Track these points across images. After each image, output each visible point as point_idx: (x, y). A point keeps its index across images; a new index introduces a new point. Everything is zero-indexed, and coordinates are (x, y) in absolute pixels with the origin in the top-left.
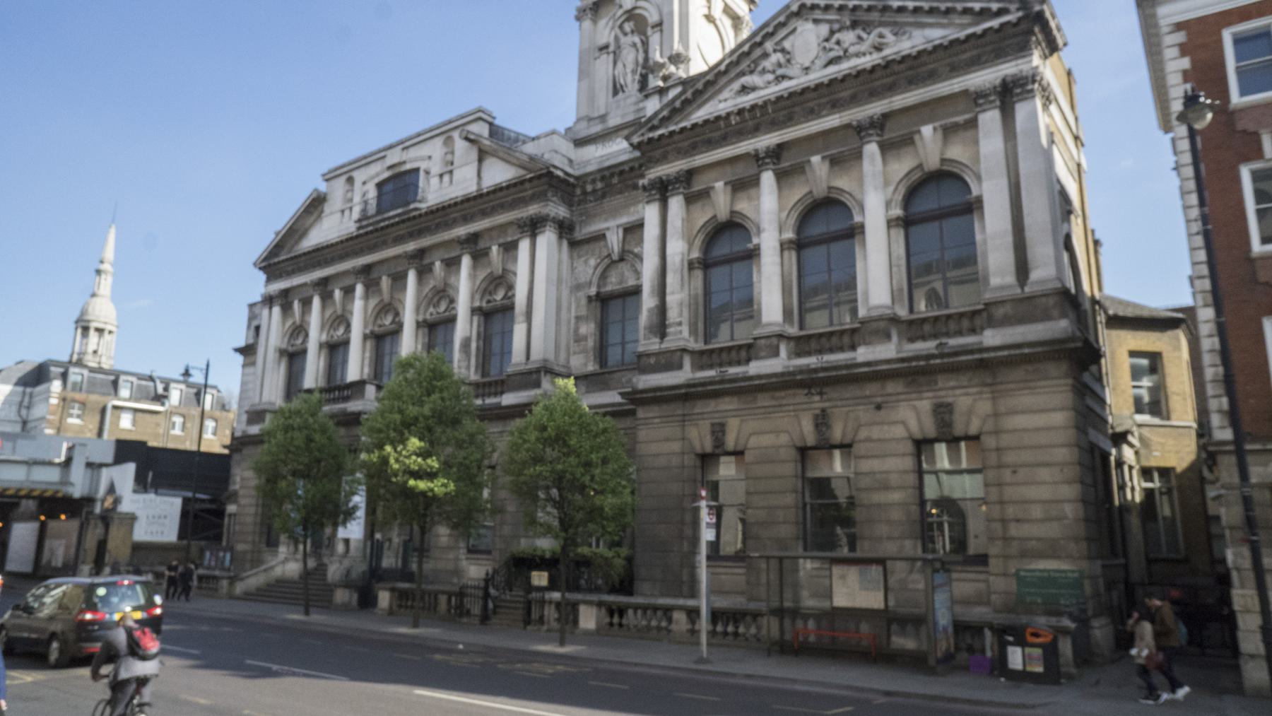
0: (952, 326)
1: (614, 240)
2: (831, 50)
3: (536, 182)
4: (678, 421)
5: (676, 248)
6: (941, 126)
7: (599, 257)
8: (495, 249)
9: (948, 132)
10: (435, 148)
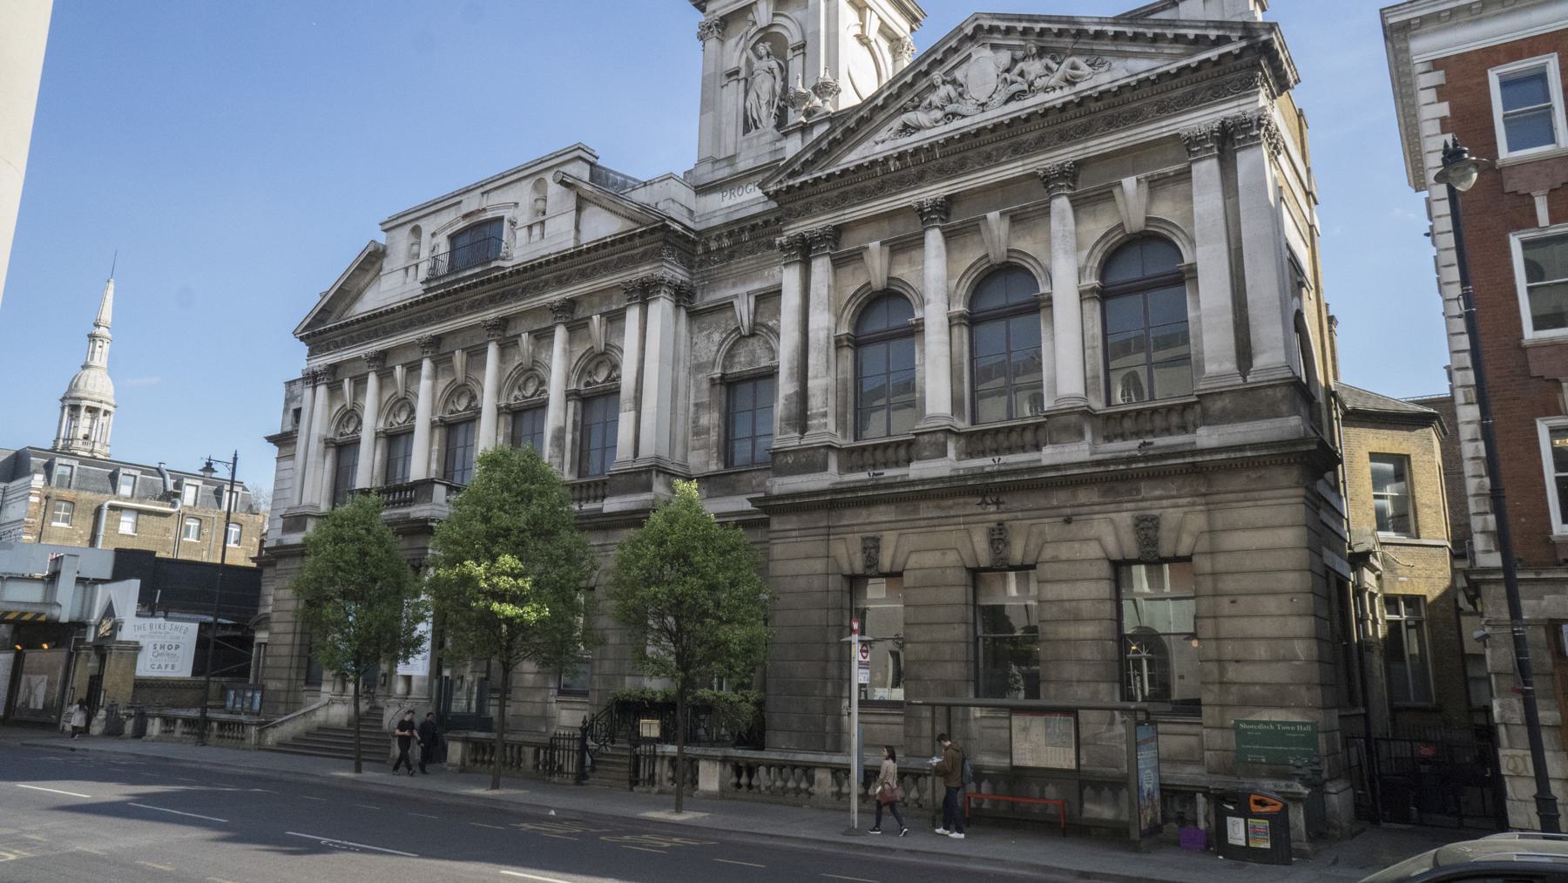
0: (1159, 422)
1: (744, 310)
2: (1013, 82)
3: (648, 238)
5: (821, 321)
6: (1147, 178)
7: (725, 331)
8: (596, 318)
9: (1155, 185)
10: (523, 194)
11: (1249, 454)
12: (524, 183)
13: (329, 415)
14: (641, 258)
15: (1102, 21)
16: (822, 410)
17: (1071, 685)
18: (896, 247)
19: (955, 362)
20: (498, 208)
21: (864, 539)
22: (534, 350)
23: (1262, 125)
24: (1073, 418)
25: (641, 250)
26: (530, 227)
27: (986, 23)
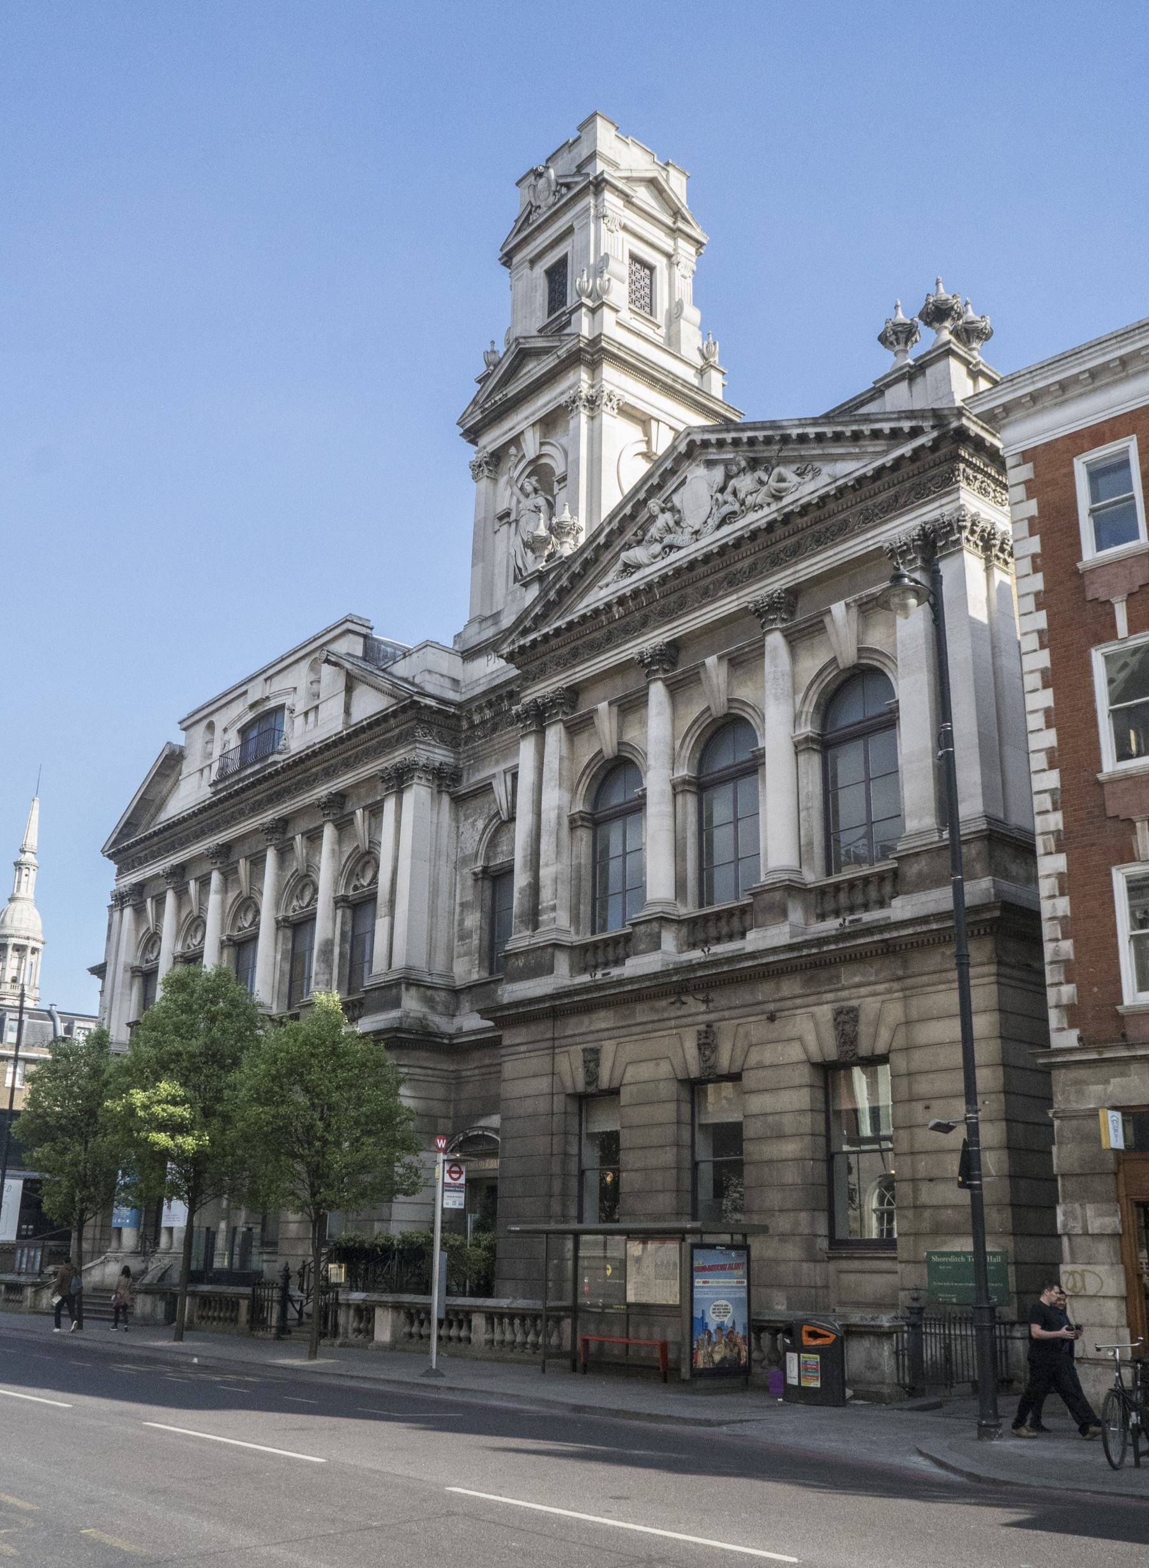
2: (726, 503)
3: (402, 717)
4: (547, 1048)
5: (553, 798)
6: (855, 601)
10: (300, 676)
11: (934, 926)
12: (297, 667)
13: (137, 937)
14: (397, 741)
15: (802, 423)
16: (551, 903)
17: (773, 1216)
18: (627, 706)
19: (679, 837)
20: (280, 695)
21: (584, 1050)
22: (307, 854)
23: (965, 527)
24: (778, 896)
25: (397, 731)
26: (306, 714)
27: (698, 438)
